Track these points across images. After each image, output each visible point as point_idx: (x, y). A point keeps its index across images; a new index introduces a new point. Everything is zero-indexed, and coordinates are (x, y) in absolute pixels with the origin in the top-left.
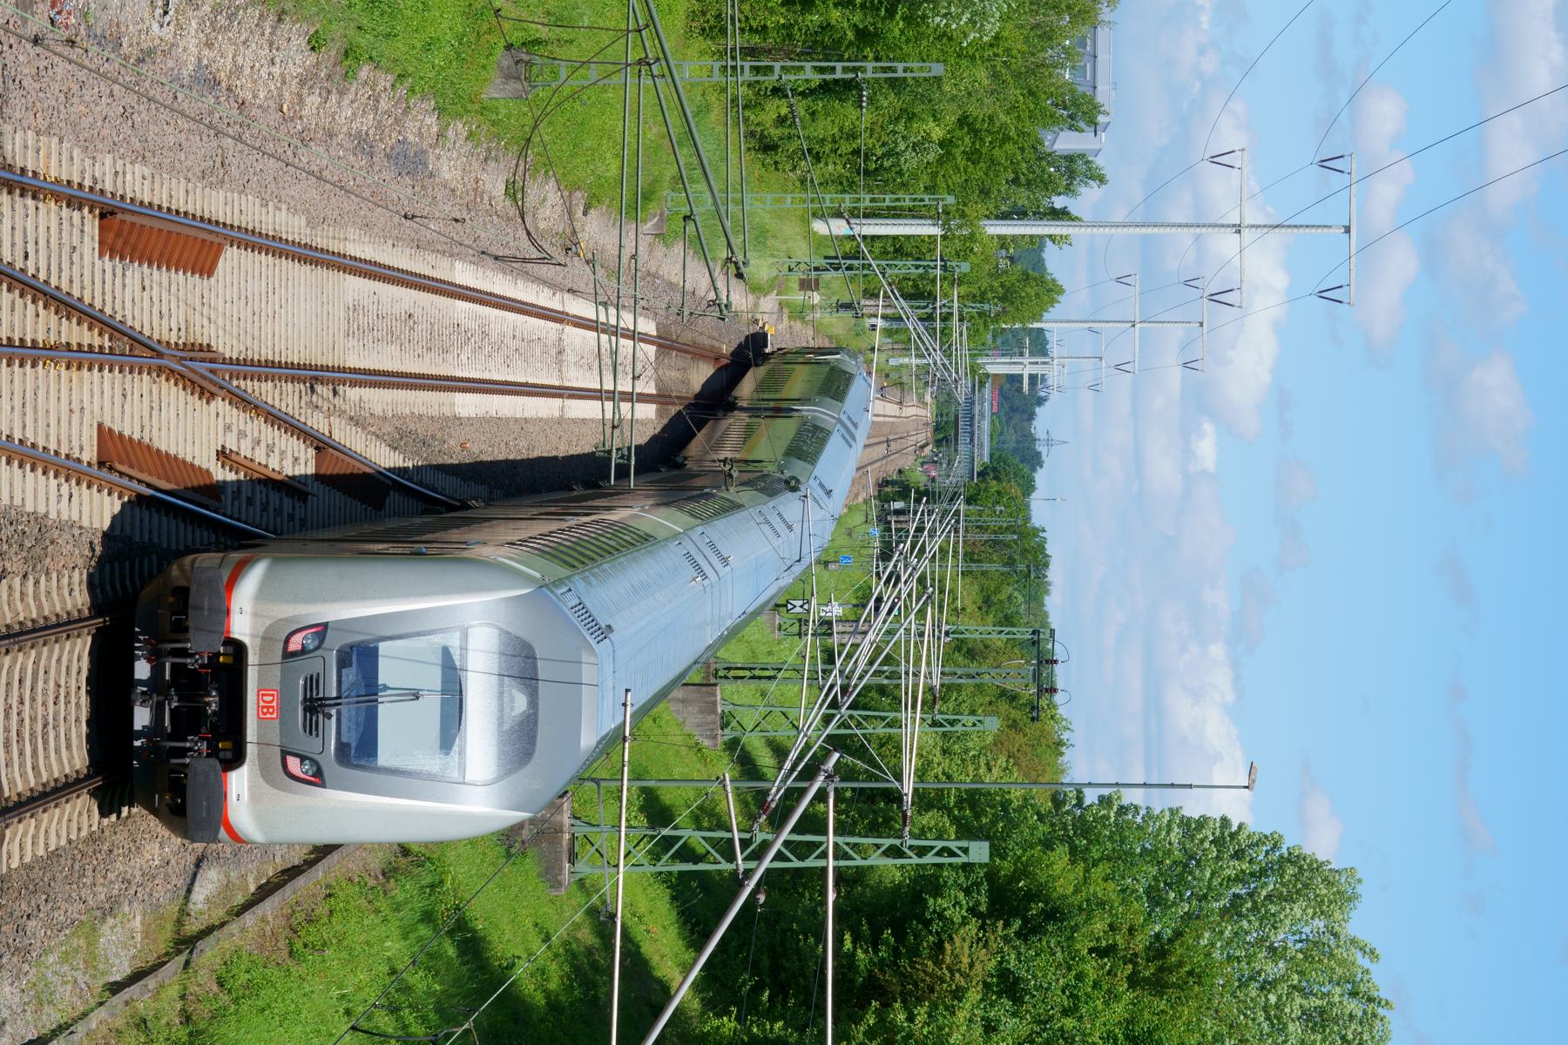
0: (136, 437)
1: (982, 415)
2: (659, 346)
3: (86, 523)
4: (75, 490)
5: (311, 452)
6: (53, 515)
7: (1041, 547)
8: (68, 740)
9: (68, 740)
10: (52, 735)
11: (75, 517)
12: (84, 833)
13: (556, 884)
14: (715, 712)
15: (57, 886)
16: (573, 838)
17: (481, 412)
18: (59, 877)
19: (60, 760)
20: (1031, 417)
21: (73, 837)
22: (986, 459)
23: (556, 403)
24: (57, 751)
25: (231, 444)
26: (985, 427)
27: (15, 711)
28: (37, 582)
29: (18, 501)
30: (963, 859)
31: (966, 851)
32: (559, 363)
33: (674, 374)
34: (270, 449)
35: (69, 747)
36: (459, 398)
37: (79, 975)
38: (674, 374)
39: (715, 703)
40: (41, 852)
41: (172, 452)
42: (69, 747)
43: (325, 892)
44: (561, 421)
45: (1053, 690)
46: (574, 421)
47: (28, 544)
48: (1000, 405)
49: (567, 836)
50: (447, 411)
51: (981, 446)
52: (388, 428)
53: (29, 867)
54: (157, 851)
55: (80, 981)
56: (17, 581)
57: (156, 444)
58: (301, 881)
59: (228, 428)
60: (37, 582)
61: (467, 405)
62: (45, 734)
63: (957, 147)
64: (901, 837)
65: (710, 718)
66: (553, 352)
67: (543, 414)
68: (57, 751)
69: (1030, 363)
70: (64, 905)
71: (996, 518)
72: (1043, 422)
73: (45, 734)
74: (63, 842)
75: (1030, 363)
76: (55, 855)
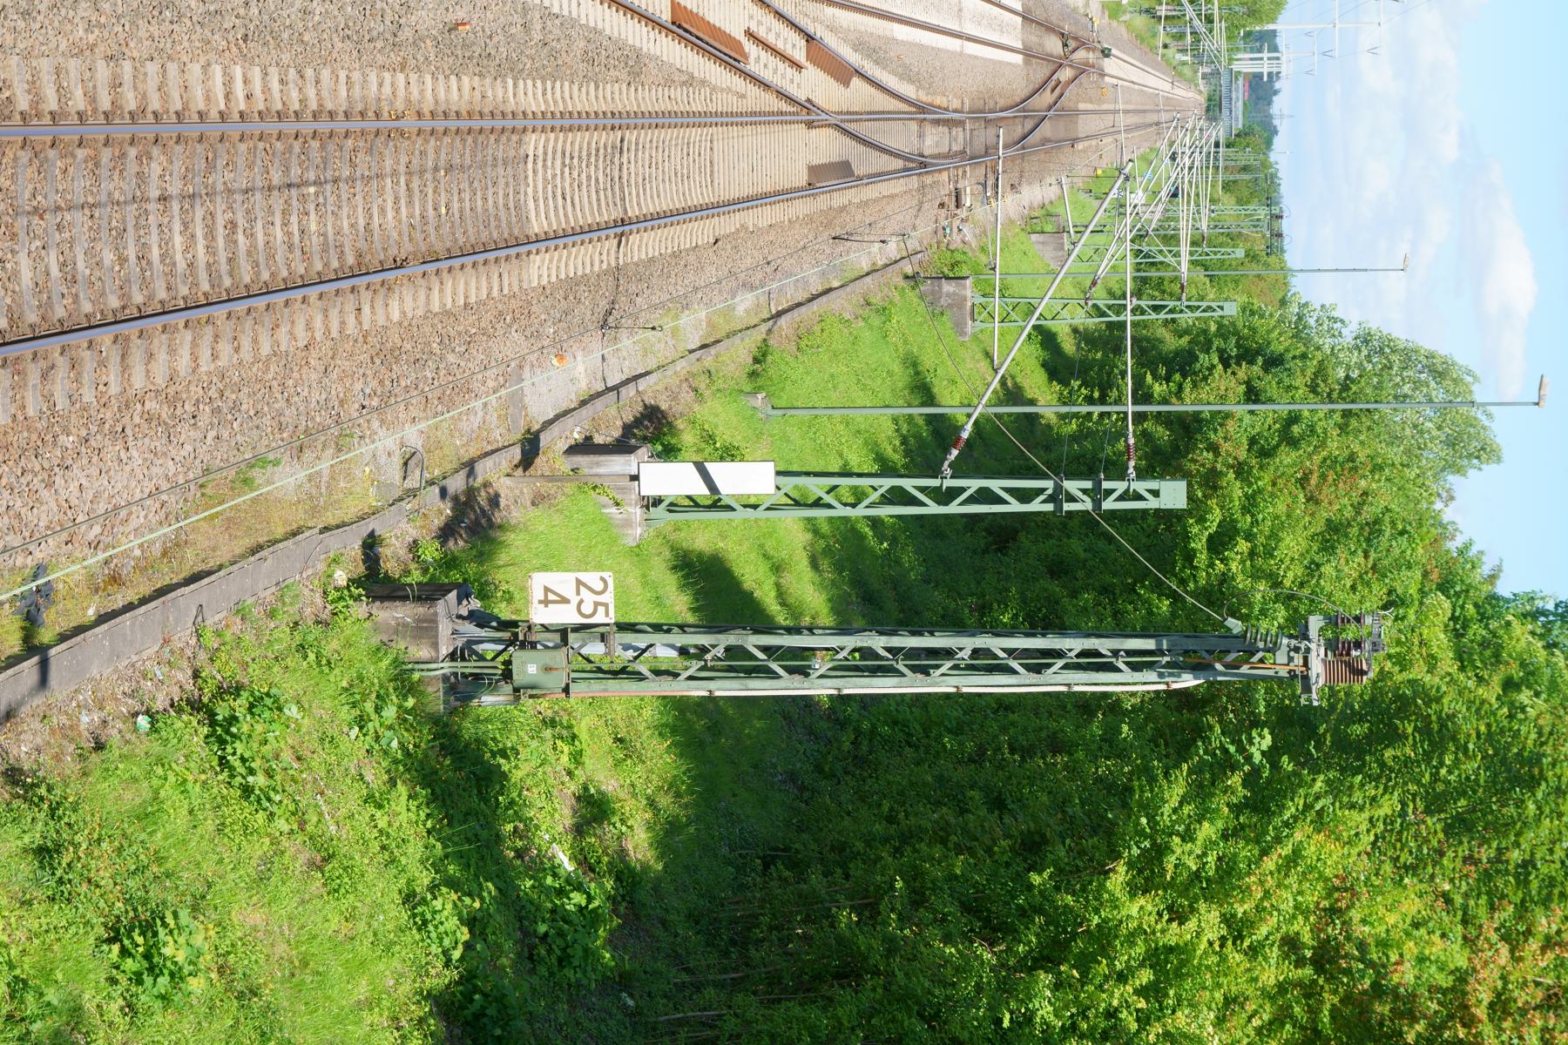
0: (695, 10)
1: (1237, 99)
2: (1024, 17)
3: (665, 59)
4: (658, 37)
5: (803, 42)
6: (645, 50)
7: (1273, 176)
8: (658, 192)
9: (658, 192)
10: (648, 186)
11: (659, 54)
12: (669, 251)
13: (962, 333)
14: (1063, 249)
15: (654, 280)
16: (973, 305)
17: (910, 39)
18: (655, 275)
19: (654, 203)
20: (1270, 103)
21: (663, 251)
22: (1240, 126)
23: (958, 42)
24: (652, 197)
25: (754, 28)
26: (1239, 107)
27: (625, 167)
28: (636, 90)
29: (623, 36)
30: (1220, 313)
31: (1222, 308)
32: (960, 17)
33: (1034, 39)
34: (778, 35)
35: (658, 196)
36: (896, 26)
37: (668, 339)
38: (1034, 39)
39: (1063, 244)
40: (643, 256)
41: (717, 25)
42: (658, 196)
43: (818, 319)
44: (961, 54)
45: (1280, 235)
46: (970, 56)
47: (630, 63)
48: (1250, 95)
49: (969, 304)
50: (888, 33)
51: (1237, 120)
52: (851, 37)
53: (637, 264)
54: (714, 272)
55: (670, 343)
56: (624, 86)
57: (707, 18)
58: (803, 309)
59: (751, 17)
60: (636, 90)
61: (902, 32)
62: (644, 185)
63: (1377, 787)
64: (1179, 299)
65: (1060, 254)
66: (956, 9)
67: (950, 48)
68: (652, 197)
69: (1269, 59)
70: (658, 293)
71: (1245, 157)
72: (1279, 105)
73: (644, 185)
74: (657, 254)
75: (1269, 59)
76: (652, 260)
